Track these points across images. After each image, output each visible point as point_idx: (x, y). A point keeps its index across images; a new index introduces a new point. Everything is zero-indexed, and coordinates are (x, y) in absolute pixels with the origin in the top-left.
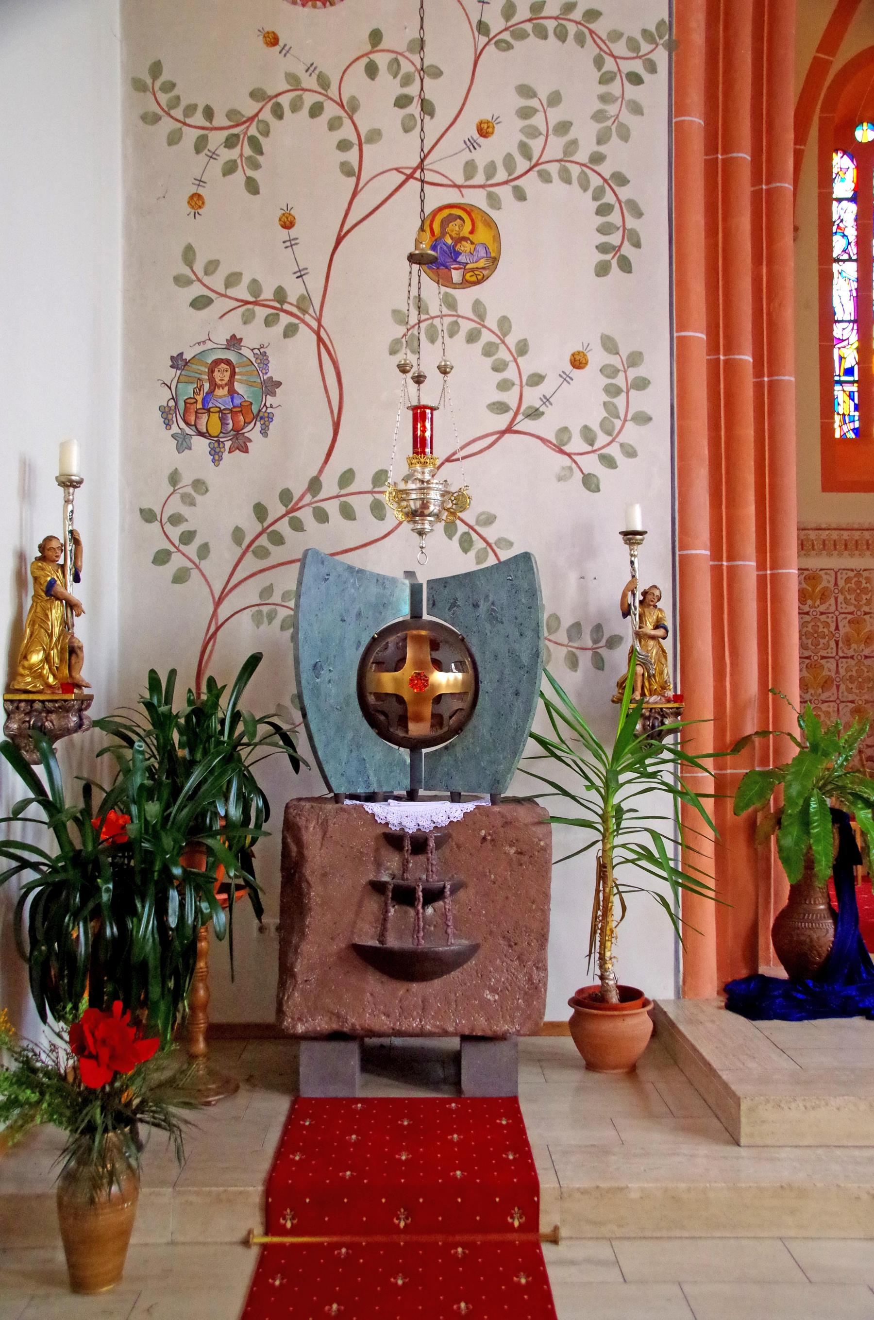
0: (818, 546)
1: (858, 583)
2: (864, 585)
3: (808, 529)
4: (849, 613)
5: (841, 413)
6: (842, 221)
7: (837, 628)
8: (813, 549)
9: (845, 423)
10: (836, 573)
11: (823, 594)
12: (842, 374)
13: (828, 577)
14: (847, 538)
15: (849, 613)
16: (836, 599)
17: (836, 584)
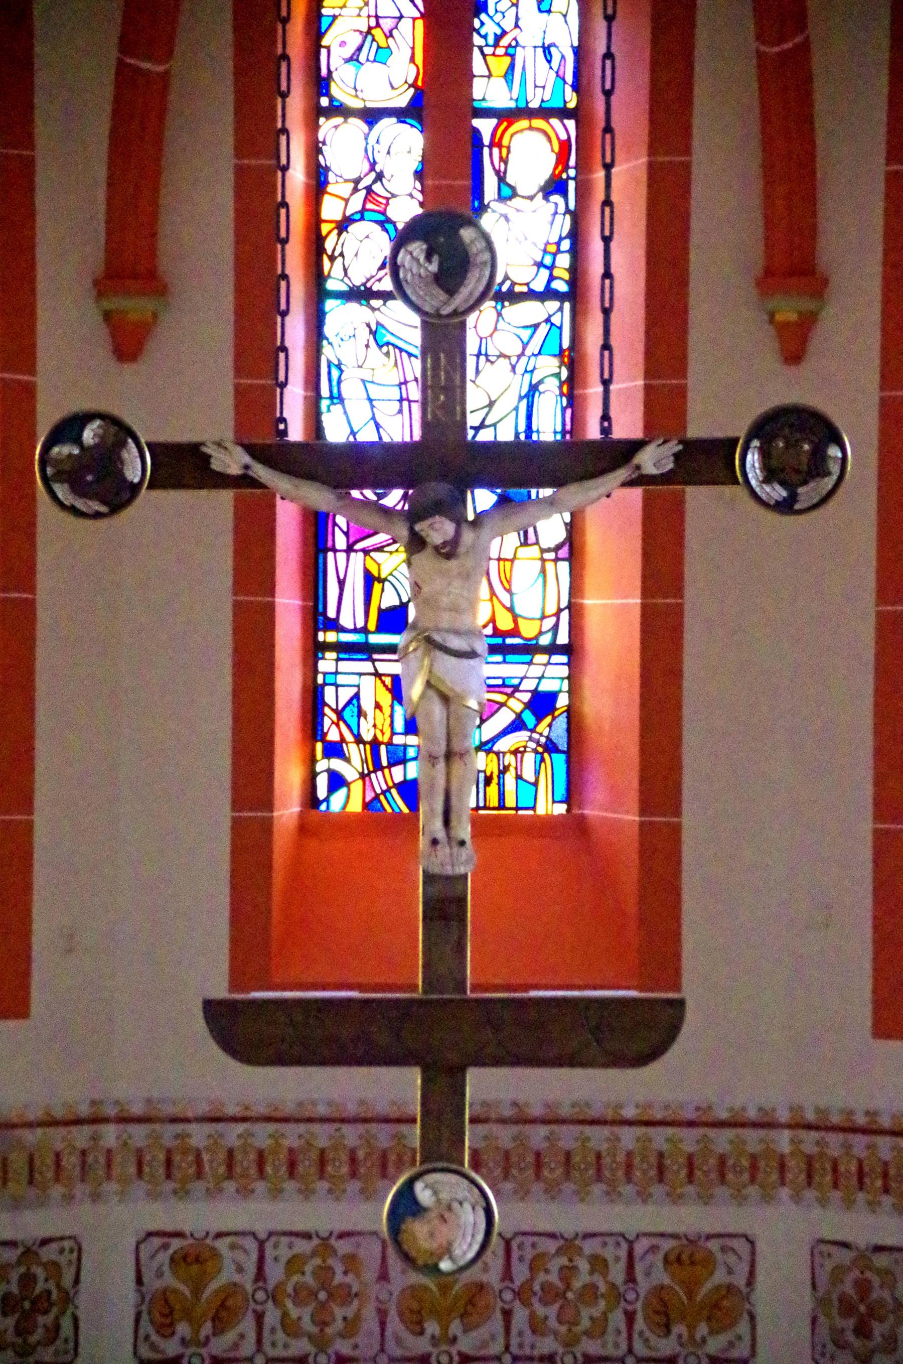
0: (214, 1165)
1: (324, 1272)
2: (339, 1278)
3: (187, 1120)
4: (383, 1324)
5: (367, 736)
6: (380, 177)
7: (631, 1278)
8: (199, 1175)
9: (378, 767)
10: (261, 1244)
11: (223, 1305)
12: (372, 626)
13: (240, 1256)
14: (296, 1143)
15: (383, 1324)
16: (259, 1318)
17: (260, 1274)
